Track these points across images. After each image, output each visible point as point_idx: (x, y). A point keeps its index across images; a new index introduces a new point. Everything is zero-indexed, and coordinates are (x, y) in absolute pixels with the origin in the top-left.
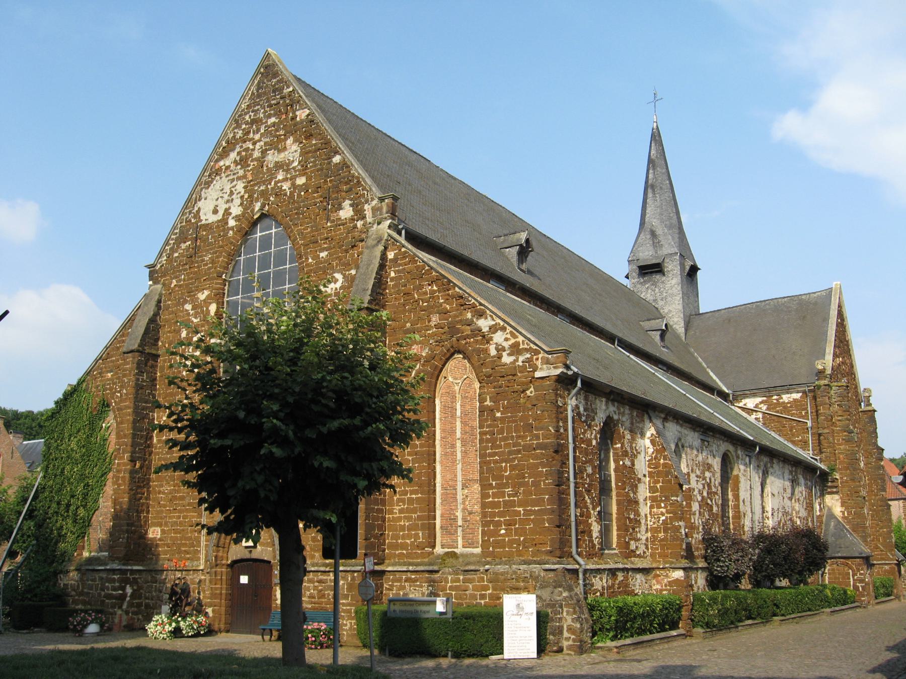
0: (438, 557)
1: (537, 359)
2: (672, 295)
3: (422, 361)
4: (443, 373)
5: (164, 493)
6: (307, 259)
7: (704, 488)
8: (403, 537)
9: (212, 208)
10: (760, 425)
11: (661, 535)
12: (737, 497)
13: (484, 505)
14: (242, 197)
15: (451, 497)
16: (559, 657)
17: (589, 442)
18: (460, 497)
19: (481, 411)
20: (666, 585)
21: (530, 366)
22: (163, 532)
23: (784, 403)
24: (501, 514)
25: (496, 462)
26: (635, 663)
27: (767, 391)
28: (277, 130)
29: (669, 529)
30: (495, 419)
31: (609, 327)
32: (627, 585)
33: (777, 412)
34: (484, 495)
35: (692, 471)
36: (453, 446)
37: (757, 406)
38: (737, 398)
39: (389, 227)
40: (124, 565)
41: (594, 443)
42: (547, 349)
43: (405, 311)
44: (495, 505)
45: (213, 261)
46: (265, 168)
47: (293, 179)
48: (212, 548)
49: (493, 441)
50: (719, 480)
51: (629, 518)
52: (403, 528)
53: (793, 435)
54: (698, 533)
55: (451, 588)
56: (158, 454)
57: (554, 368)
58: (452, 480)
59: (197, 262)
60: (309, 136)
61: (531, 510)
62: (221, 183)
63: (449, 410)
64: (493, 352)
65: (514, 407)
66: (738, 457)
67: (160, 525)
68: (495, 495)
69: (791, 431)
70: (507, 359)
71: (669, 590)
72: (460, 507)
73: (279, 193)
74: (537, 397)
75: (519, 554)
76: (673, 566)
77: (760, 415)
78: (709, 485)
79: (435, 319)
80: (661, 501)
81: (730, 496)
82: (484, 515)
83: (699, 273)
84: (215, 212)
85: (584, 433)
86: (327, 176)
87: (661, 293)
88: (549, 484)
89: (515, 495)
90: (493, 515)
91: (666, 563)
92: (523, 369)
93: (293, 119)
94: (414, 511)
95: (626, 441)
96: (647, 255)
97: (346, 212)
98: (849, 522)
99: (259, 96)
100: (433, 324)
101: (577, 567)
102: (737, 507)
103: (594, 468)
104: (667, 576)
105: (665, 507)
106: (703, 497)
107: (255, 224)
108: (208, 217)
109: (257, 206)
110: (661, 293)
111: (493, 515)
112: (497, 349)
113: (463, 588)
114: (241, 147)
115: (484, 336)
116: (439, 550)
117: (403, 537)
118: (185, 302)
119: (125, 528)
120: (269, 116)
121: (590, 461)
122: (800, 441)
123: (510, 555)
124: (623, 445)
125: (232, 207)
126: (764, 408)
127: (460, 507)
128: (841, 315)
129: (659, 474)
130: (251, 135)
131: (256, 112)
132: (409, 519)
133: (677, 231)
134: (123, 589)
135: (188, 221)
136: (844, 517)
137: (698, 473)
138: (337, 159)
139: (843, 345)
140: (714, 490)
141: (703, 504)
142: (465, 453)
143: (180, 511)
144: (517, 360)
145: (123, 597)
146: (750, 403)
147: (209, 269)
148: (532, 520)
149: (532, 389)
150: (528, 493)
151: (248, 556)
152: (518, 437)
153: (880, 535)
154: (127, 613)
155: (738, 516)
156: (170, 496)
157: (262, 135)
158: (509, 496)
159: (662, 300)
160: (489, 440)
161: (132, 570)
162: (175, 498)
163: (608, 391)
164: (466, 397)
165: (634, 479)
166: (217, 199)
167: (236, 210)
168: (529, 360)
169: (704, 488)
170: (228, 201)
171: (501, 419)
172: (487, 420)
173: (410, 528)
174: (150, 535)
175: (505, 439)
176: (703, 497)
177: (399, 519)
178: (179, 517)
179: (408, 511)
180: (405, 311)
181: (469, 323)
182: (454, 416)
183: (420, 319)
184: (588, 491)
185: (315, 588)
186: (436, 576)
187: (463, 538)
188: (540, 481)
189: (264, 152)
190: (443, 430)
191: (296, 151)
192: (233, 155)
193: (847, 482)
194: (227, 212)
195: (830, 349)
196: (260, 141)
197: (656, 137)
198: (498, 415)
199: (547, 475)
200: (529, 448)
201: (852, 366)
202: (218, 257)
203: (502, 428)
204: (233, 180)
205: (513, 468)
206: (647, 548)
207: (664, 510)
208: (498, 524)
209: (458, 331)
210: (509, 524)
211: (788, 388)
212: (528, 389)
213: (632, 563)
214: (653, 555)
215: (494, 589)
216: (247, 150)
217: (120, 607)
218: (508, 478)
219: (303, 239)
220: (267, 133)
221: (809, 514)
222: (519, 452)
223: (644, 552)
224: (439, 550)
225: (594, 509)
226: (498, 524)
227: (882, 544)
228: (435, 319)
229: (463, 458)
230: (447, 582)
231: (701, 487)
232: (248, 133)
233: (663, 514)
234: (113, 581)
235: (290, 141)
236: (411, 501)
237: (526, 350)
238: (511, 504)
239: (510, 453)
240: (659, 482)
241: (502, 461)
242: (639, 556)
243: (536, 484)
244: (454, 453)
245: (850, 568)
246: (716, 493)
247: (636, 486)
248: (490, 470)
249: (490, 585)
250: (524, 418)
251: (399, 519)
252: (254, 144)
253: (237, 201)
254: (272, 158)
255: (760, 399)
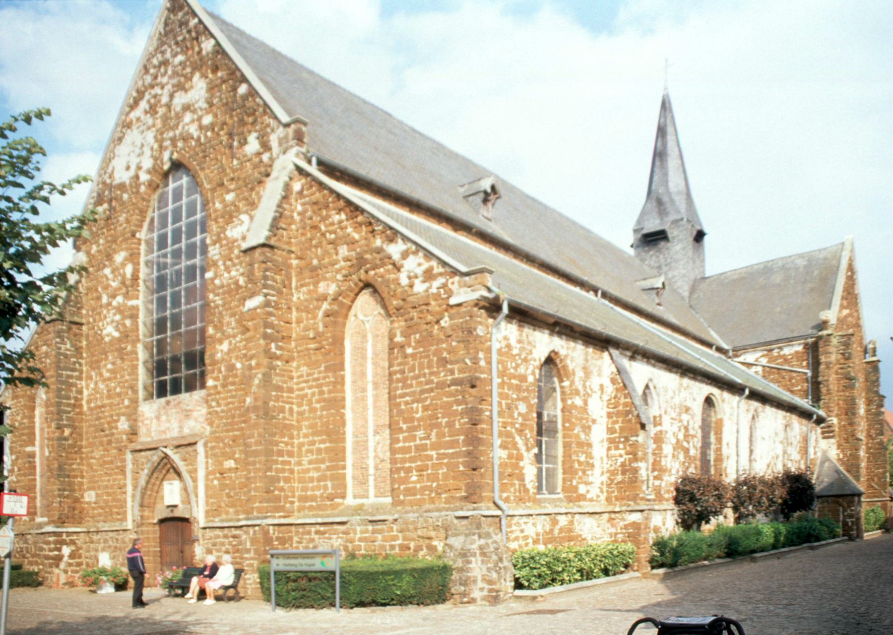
0: (349, 507)
1: (453, 283)
2: (677, 261)
3: (329, 298)
4: (352, 312)
5: (94, 458)
6: (214, 203)
7: (680, 430)
8: (313, 489)
9: (125, 165)
10: (759, 377)
11: (619, 478)
12: (719, 440)
13: (393, 451)
14: (152, 149)
15: (361, 446)
16: (471, 607)
17: (523, 378)
18: (371, 445)
19: (391, 349)
20: (621, 529)
21: (445, 293)
22: (97, 495)
23: (784, 355)
24: (412, 460)
25: (406, 403)
26: (549, 616)
27: (767, 345)
28: (184, 69)
29: (627, 471)
30: (406, 356)
31: (594, 281)
32: (570, 530)
33: (778, 364)
34: (394, 440)
35: (666, 412)
36: (364, 390)
37: (756, 360)
38: (737, 351)
39: (297, 155)
40: (58, 527)
41: (531, 379)
42: (464, 269)
43: (311, 246)
44: (406, 450)
45: (128, 221)
46: (173, 112)
47: (200, 119)
48: (137, 508)
49: (404, 380)
50: (699, 422)
51: (579, 461)
52: (311, 480)
53: (793, 385)
54: (670, 476)
55: (360, 540)
56: (87, 421)
57: (473, 291)
58: (363, 426)
59: (113, 224)
60: (215, 69)
61: (444, 454)
62: (133, 136)
63: (360, 352)
64: (404, 281)
65: (427, 340)
66: (723, 401)
67: (93, 489)
68: (405, 440)
69: (790, 381)
70: (419, 287)
71: (624, 534)
72: (371, 454)
73: (186, 138)
74: (453, 328)
75: (432, 501)
76: (629, 509)
77: (760, 369)
78: (686, 429)
79: (343, 251)
80: (620, 442)
81: (713, 438)
82: (393, 461)
83: (706, 238)
84: (128, 168)
85: (516, 368)
86: (234, 110)
87: (666, 259)
88: (465, 423)
89: (428, 437)
90: (404, 461)
91: (621, 506)
92: (437, 297)
93: (200, 52)
94: (322, 461)
95: (577, 379)
96: (653, 225)
97: (253, 145)
98: (843, 464)
99: (166, 34)
100: (340, 257)
101: (499, 513)
102: (719, 450)
103: (529, 406)
104: (623, 519)
105: (625, 448)
106: (678, 440)
107: (166, 175)
108: (122, 176)
109: (166, 156)
110: (666, 259)
111: (404, 461)
112: (410, 278)
113: (372, 539)
114: (150, 94)
115: (394, 264)
116: (350, 501)
117: (313, 489)
118: (105, 266)
119: (56, 493)
120: (175, 55)
121: (525, 399)
122: (800, 390)
123: (420, 503)
124: (572, 383)
125: (143, 161)
126: (764, 361)
127: (371, 454)
128: (851, 268)
129: (618, 414)
130: (159, 79)
131: (163, 53)
132: (318, 470)
133: (684, 197)
134: (60, 550)
135: (104, 183)
136: (839, 460)
137: (674, 415)
138: (243, 89)
139: (851, 297)
140: (691, 432)
141: (678, 446)
142: (376, 397)
143: (110, 475)
144: (430, 287)
145: (59, 558)
146: (750, 357)
147: (125, 229)
148: (446, 464)
149: (446, 318)
150: (440, 435)
151: (171, 515)
152: (432, 374)
153: (875, 475)
154: (66, 572)
155: (719, 459)
156: (101, 461)
157: (170, 77)
158: (421, 439)
159: (666, 265)
160: (393, 380)
161: (67, 532)
162: (105, 462)
163: (552, 321)
164: (377, 336)
165: (587, 419)
166: (129, 155)
167: (148, 163)
168: (444, 286)
169: (680, 430)
170: (139, 155)
171: (413, 356)
172: (397, 358)
173: (319, 480)
174: (87, 499)
175: (416, 377)
176: (678, 440)
177: (308, 471)
178: (109, 481)
179: (317, 461)
180: (311, 246)
181: (379, 251)
182: (364, 357)
183: (326, 253)
184: (520, 432)
185: (230, 543)
186: (347, 526)
187: (376, 487)
188: (454, 421)
189: (172, 96)
190: (354, 374)
191: (202, 88)
192: (143, 105)
193: (844, 426)
194: (139, 168)
195: (837, 300)
196: (167, 84)
197: (665, 106)
198: (409, 351)
199: (462, 414)
200: (441, 385)
201: (858, 318)
202: (132, 215)
203: (414, 365)
204: (143, 132)
205: (425, 408)
206: (602, 491)
207: (623, 452)
208: (408, 471)
209: (366, 261)
210: (420, 469)
211: (789, 340)
212: (441, 319)
213: (580, 506)
214: (608, 499)
215: (404, 539)
216: (155, 96)
217: (57, 566)
218: (419, 420)
219: (209, 183)
220: (175, 74)
221: (802, 458)
222: (432, 390)
223: (598, 496)
224: (350, 501)
225: (528, 450)
226: (408, 471)
227: (876, 483)
228: (343, 251)
229: (375, 402)
230: (355, 533)
231: (676, 430)
232: (156, 77)
233: (621, 456)
234: (48, 543)
235: (197, 76)
236: (319, 451)
237: (441, 274)
238: (423, 448)
239: (422, 392)
240: (617, 422)
241: (413, 402)
242: (591, 500)
243: (450, 425)
244: (364, 398)
245: (841, 505)
246: (693, 436)
247: (589, 428)
248: (401, 412)
249: (400, 535)
250: (437, 353)
251: (308, 471)
252: (162, 88)
253: (148, 153)
254: (180, 100)
255: (759, 354)
